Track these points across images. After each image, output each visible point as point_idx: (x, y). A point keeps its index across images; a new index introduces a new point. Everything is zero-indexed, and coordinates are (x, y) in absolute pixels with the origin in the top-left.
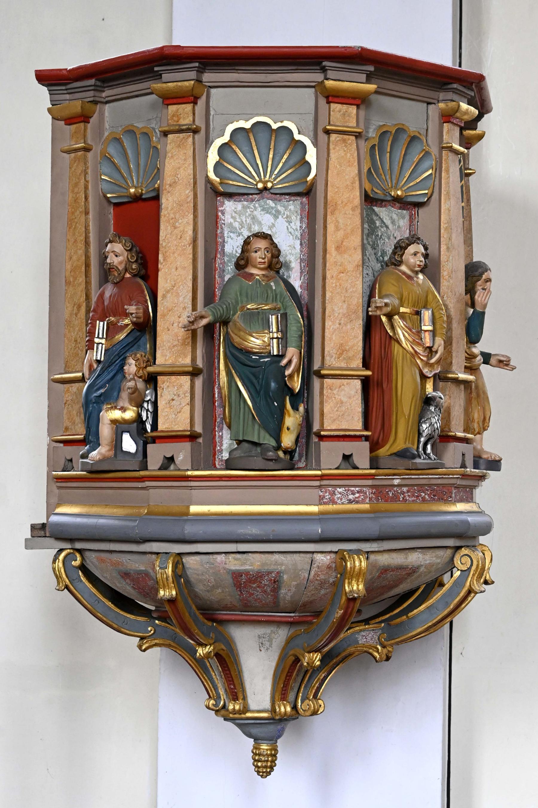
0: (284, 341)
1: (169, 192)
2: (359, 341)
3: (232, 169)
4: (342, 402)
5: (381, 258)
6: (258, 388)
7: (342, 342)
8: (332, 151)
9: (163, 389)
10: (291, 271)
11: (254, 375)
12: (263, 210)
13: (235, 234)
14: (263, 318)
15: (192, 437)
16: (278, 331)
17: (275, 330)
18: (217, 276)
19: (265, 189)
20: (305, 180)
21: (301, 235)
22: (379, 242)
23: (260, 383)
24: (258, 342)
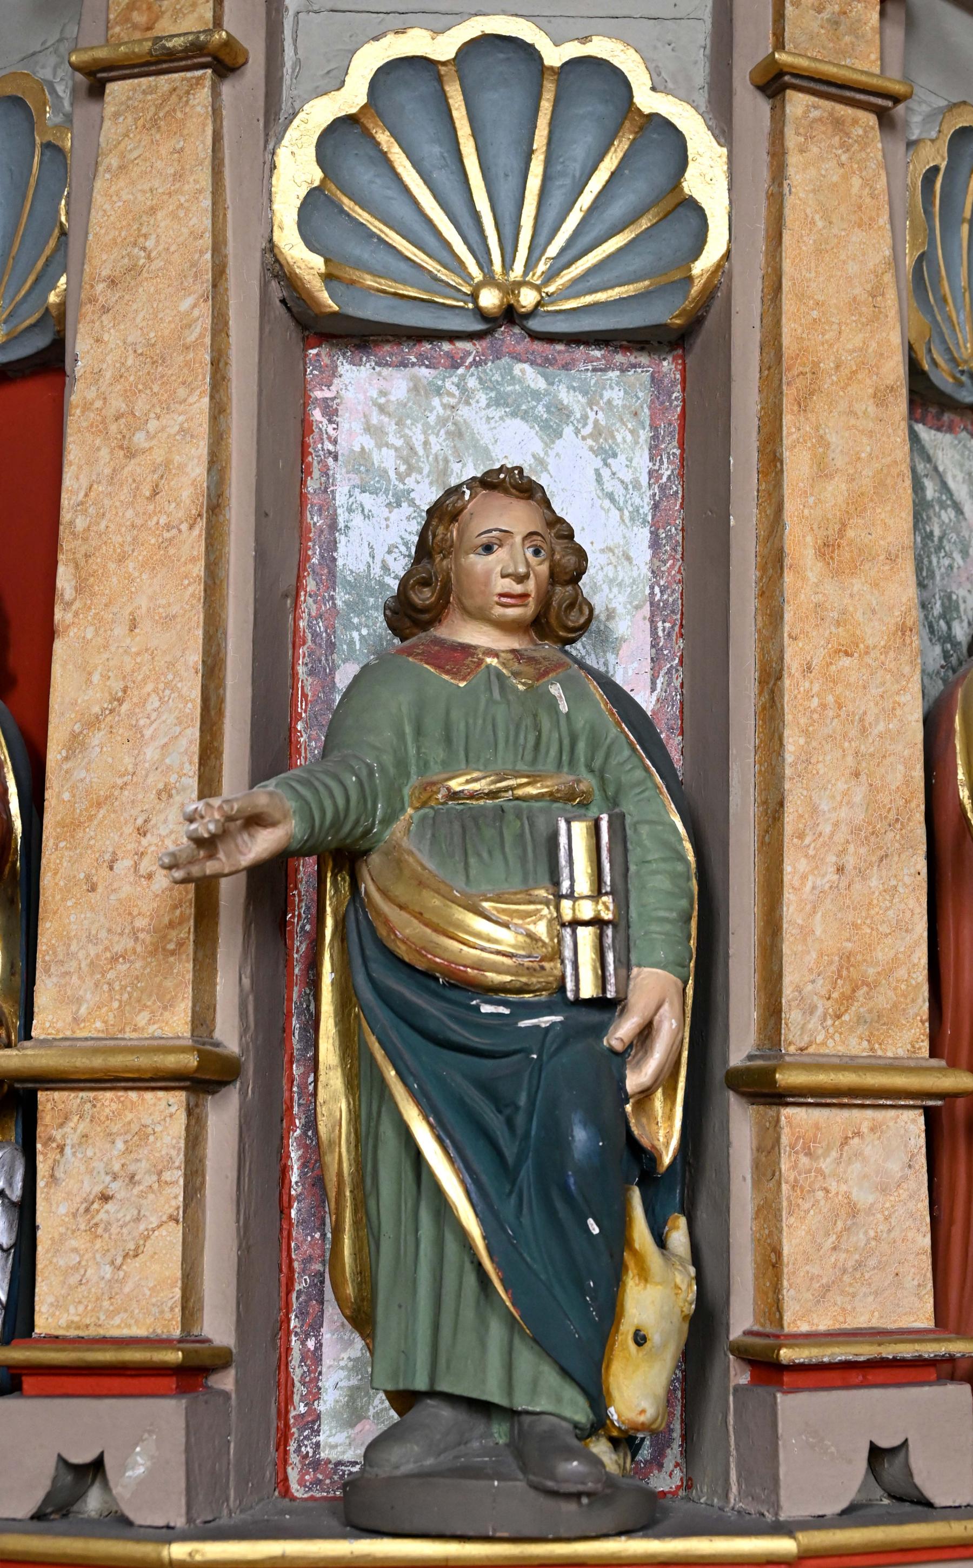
0: (617, 935)
1: (105, 310)
2: (917, 943)
3: (376, 226)
4: (853, 1211)
5: (942, 623)
6: (510, 1153)
7: (849, 945)
8: (794, 160)
9: (61, 1148)
10: (616, 650)
11: (487, 1088)
12: (499, 401)
13: (382, 499)
14: (521, 835)
15: (190, 1373)
16: (598, 893)
17: (583, 885)
18: (301, 669)
19: (510, 315)
20: (678, 276)
21: (656, 506)
22: (934, 560)
23: (520, 1131)
24: (507, 938)
